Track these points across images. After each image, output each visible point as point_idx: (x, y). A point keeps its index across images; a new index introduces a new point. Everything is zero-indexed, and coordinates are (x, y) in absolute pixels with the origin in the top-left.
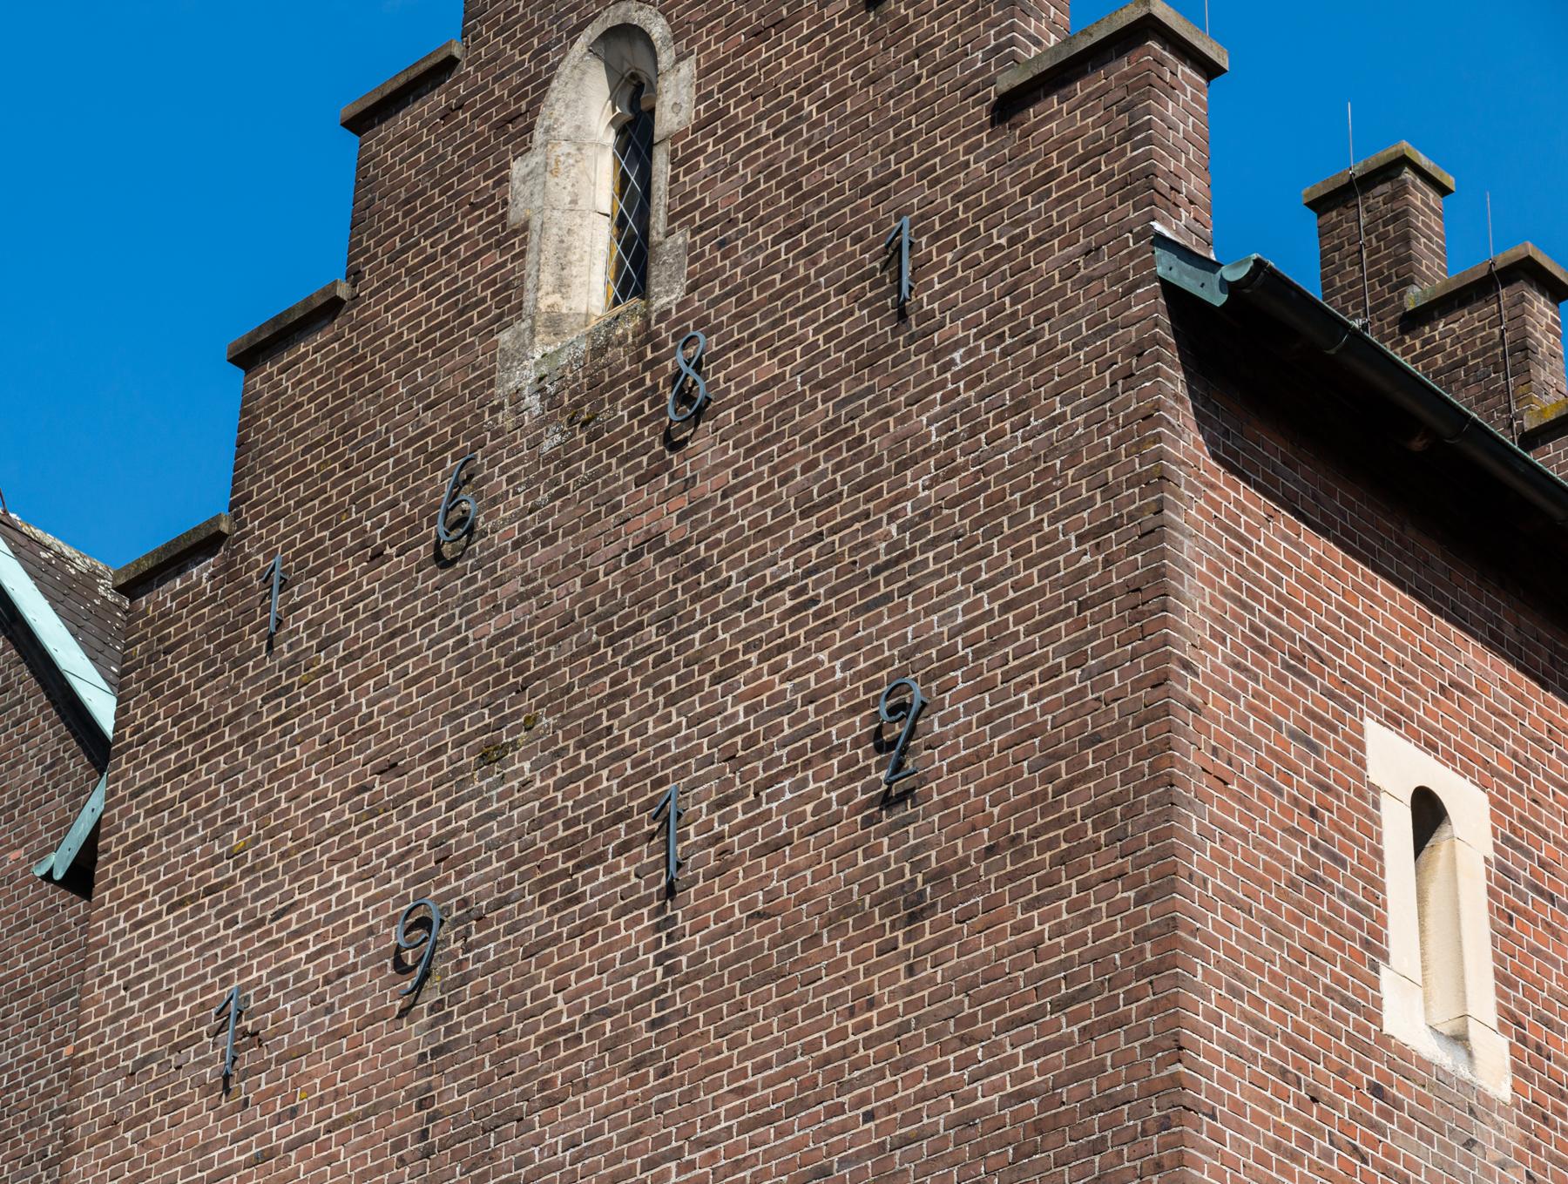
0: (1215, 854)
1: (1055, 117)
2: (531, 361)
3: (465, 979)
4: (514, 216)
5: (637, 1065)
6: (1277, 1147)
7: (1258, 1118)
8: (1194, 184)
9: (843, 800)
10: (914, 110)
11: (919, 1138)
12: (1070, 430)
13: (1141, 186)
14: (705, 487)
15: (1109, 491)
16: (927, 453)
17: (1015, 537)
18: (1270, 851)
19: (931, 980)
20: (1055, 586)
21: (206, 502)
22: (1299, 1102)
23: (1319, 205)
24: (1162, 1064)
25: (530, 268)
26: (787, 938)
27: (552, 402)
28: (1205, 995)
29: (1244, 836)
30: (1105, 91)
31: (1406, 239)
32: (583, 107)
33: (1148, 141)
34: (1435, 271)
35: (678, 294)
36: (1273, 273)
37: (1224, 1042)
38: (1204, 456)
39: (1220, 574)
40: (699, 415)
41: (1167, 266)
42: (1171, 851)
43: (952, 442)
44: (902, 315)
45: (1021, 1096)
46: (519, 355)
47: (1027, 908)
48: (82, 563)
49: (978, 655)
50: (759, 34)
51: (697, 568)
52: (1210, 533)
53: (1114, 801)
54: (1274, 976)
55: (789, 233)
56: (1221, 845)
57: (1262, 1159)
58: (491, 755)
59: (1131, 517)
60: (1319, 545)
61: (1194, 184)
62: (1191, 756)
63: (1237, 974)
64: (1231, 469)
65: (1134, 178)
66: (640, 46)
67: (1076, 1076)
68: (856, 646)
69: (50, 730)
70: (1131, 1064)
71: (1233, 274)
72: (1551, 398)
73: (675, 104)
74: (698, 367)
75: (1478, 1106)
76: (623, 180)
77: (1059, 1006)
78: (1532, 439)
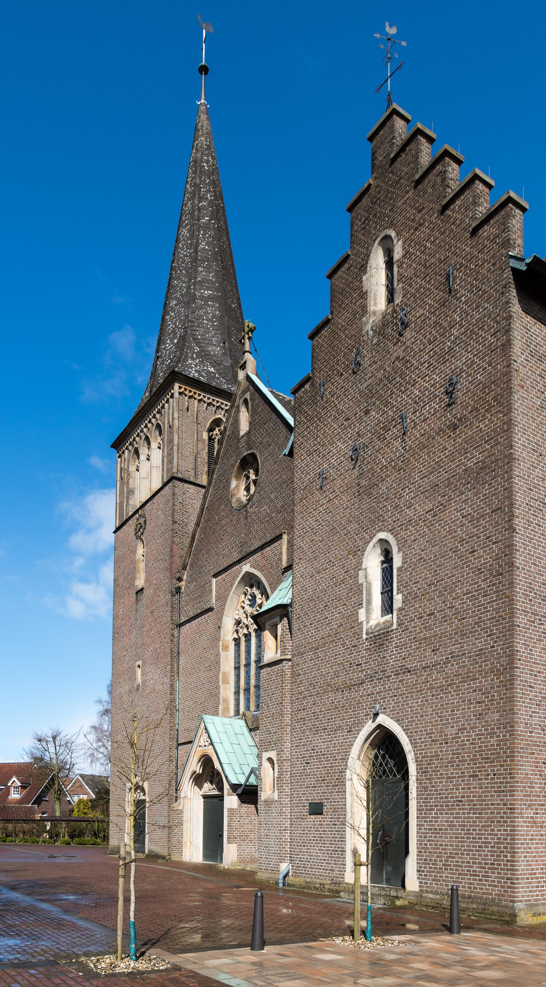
0: (521, 404)
1: (487, 231)
2: (370, 322)
3: (365, 459)
4: (364, 290)
5: (399, 470)
6: (532, 466)
7: (528, 460)
8: (519, 241)
9: (439, 407)
10: (452, 239)
11: (456, 475)
12: (489, 310)
13: (507, 244)
14: (408, 343)
15: (498, 323)
16: (456, 324)
17: (476, 339)
18: (533, 402)
19: (459, 442)
20: (485, 348)
21: (307, 371)
22: (537, 456)
24: (508, 451)
25: (368, 301)
26: (428, 439)
27: (375, 331)
28: (518, 435)
29: (527, 399)
30: (498, 221)
32: (378, 259)
33: (508, 231)
35: (400, 299)
37: (521, 444)
39: (523, 338)
40: (406, 327)
41: (513, 263)
42: (511, 404)
43: (462, 320)
44: (450, 291)
45: (478, 463)
46: (367, 322)
47: (479, 422)
49: (468, 368)
50: (416, 229)
51: (407, 362)
52: (521, 329)
53: (498, 395)
54: (533, 430)
55: (424, 278)
57: (529, 468)
58: (367, 412)
59: (503, 328)
61: (519, 241)
62: (516, 382)
63: (525, 430)
64: (526, 313)
65: (505, 242)
66: (389, 240)
67: (489, 456)
68: (441, 372)
69: (282, 426)
70: (501, 452)
71: (528, 261)
73: (398, 253)
74: (405, 316)
76: (387, 276)
77: (485, 442)
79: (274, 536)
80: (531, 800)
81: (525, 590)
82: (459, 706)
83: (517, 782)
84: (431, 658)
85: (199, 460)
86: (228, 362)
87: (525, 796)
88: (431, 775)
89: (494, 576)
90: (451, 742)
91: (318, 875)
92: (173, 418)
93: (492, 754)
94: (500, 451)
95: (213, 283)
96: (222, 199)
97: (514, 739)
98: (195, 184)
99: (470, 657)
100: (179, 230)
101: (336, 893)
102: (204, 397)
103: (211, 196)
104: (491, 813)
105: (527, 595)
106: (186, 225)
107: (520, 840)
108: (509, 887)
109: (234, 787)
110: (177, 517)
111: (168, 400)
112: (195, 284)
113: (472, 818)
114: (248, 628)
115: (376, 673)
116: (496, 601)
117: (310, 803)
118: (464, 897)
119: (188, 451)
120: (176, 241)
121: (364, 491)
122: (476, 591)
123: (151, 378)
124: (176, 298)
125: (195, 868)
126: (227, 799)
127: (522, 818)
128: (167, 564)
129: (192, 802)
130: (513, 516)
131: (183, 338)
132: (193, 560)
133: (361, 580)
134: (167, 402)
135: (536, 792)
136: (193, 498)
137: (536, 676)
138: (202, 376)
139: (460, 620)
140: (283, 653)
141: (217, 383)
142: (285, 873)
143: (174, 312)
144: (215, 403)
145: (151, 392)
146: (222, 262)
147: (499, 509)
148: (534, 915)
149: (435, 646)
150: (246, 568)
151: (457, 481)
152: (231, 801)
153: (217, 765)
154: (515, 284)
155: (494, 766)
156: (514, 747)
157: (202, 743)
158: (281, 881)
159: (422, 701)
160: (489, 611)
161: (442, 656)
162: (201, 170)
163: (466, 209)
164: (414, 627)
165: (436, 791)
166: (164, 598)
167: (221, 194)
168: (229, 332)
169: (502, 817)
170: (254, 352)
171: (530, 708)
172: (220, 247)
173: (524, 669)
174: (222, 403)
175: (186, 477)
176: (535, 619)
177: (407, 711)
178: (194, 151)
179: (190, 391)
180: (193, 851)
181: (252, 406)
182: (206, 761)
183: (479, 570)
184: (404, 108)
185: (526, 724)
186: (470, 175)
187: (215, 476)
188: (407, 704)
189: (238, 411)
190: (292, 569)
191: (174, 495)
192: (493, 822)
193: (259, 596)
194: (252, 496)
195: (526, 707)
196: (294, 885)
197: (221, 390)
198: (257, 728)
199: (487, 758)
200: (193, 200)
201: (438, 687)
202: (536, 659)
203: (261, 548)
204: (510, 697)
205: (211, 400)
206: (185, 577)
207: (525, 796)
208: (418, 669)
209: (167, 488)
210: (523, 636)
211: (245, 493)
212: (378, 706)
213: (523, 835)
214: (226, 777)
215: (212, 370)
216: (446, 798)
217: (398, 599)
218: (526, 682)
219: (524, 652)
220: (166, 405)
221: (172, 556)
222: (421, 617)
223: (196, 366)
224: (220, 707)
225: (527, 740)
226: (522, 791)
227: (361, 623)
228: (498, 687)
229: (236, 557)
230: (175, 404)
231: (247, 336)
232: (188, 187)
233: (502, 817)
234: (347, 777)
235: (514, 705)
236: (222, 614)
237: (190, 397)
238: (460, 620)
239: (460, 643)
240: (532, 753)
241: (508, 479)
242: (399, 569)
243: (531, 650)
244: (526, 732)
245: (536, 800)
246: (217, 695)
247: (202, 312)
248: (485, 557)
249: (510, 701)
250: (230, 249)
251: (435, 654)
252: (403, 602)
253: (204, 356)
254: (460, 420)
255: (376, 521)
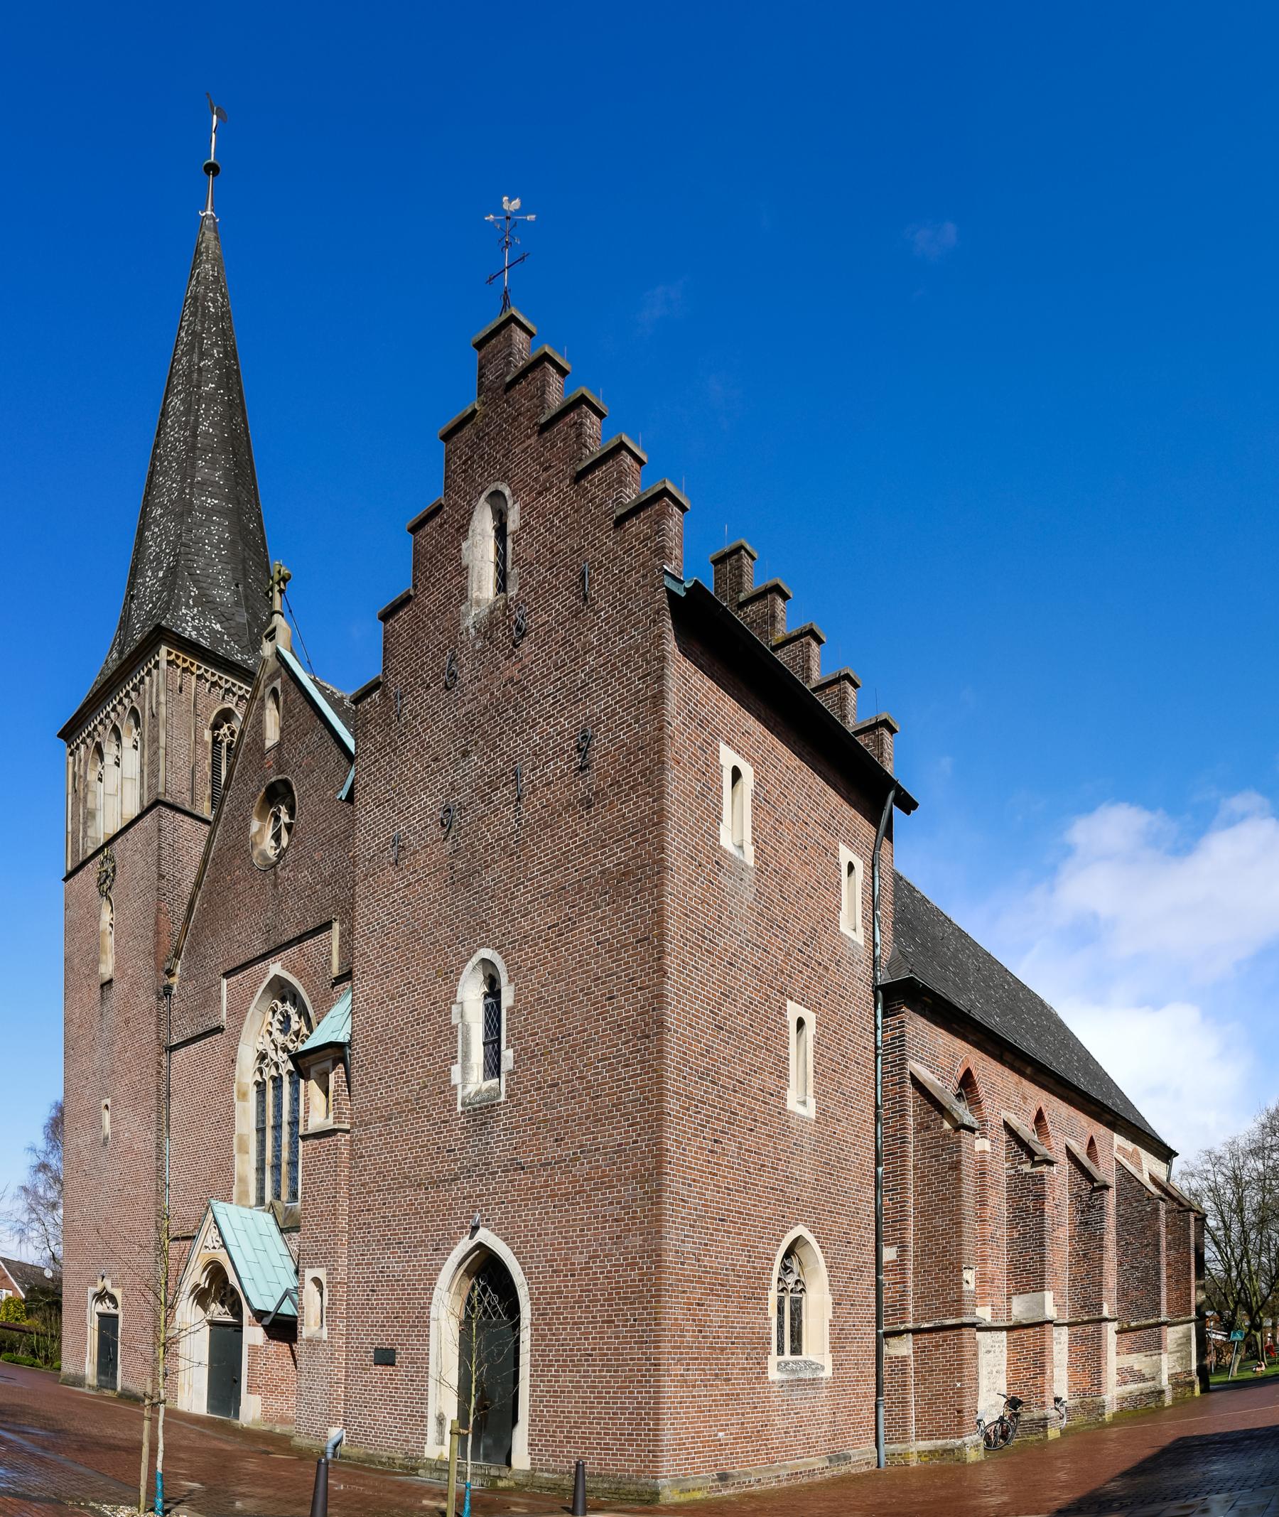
1: (636, 526)
2: (472, 616)
21: (375, 672)
23: (715, 562)
27: (478, 631)
30: (650, 516)
31: (741, 576)
32: (484, 522)
34: (751, 586)
35: (516, 591)
36: (700, 585)
38: (677, 651)
41: (669, 583)
44: (585, 599)
45: (619, 864)
46: (467, 614)
48: (339, 695)
50: (540, 494)
56: (677, 782)
57: (685, 884)
58: (465, 754)
60: (710, 683)
61: (677, 552)
62: (670, 754)
67: (634, 858)
69: (336, 751)
71: (688, 586)
72: (780, 635)
73: (513, 522)
75: (745, 868)
76: (498, 549)
78: (775, 648)
79: (318, 923)
80: (681, 1353)
81: (678, 1063)
82: (591, 1224)
83: (664, 1330)
84: (553, 1152)
85: (198, 775)
86: (243, 618)
87: (673, 1347)
88: (551, 1319)
89: (639, 1039)
90: (580, 1275)
91: (385, 1443)
92: (158, 703)
93: (632, 1293)
94: (648, 852)
95: (219, 487)
96: (235, 358)
97: (661, 1272)
98: (194, 332)
99: (606, 1154)
100: (166, 399)
101: (414, 1470)
102: (207, 671)
103: (219, 353)
104: (630, 1370)
105: (680, 1070)
106: (179, 392)
107: (666, 1404)
108: (650, 1461)
109: (259, 1315)
110: (165, 868)
111: (150, 670)
112: (191, 485)
113: (605, 1377)
114: (277, 1068)
115: (477, 1166)
116: (640, 1075)
117: (376, 1349)
118: (592, 1475)
119: (182, 759)
120: (162, 415)
121: (461, 880)
122: (614, 1057)
123: (120, 629)
124: (162, 505)
125: (197, 1420)
126: (247, 1329)
127: (670, 1375)
128: (149, 944)
129: (193, 1327)
130: (663, 952)
131: (172, 571)
132: (191, 942)
133: (455, 1020)
134: (149, 673)
135: (688, 1342)
136: (190, 840)
137: (690, 1185)
138: (202, 636)
139: (592, 1099)
140: (337, 1119)
141: (225, 649)
142: (336, 1440)
143: (158, 526)
144: (222, 683)
145: (121, 653)
146: (235, 455)
147: (646, 939)
148: (682, 1491)
149: (559, 1134)
150: (275, 968)
151: (591, 888)
152: (253, 1335)
153: (232, 1279)
154: (671, 611)
155: (635, 1309)
156: (661, 1284)
157: (209, 1243)
158: (330, 1451)
159: (540, 1214)
160: (631, 1089)
161: (569, 1149)
162: (203, 312)
163: (610, 486)
164: (530, 1102)
165: (557, 1340)
166: (146, 1000)
167: (235, 350)
168: (244, 568)
169: (643, 1376)
170: (288, 613)
171: (683, 1230)
172: (232, 431)
173: (675, 1176)
174: (234, 685)
175: (178, 802)
176: (690, 1105)
177: (519, 1227)
178: (194, 282)
179: (185, 660)
180: (193, 1396)
181: (285, 702)
182: (216, 1271)
183: (619, 1026)
184: (526, 316)
185: (677, 1252)
186: (614, 442)
187: (225, 809)
188: (520, 1216)
189: (262, 707)
190: (350, 979)
191: (160, 830)
192: (632, 1382)
193: (295, 1018)
194: (285, 850)
195: (677, 1229)
196: (349, 1458)
197: (232, 662)
198: (296, 1229)
199: (625, 1298)
200: (191, 356)
201: (562, 1195)
202: (690, 1162)
203: (299, 939)
204: (656, 1215)
205: (216, 678)
206: (178, 971)
207: (673, 1347)
208: (535, 1166)
209: (148, 817)
210: (675, 1129)
211: (273, 843)
212: (478, 1216)
213: (670, 1397)
214: (247, 1299)
215: (218, 627)
216: (571, 1350)
217: (508, 1055)
218: (677, 1194)
219: (675, 1152)
220: (147, 679)
221: (157, 933)
222: (540, 1088)
223: (193, 619)
224: (235, 1189)
225: (677, 1274)
226: (670, 1341)
227: (455, 1087)
228: (642, 1199)
229: (259, 949)
230: (161, 679)
231: (277, 588)
232: (183, 334)
233: (643, 1376)
234: (432, 1315)
235: (661, 1226)
236: (238, 1039)
237: (185, 670)
238: (592, 1099)
239: (593, 1133)
240: (684, 1292)
241: (659, 897)
242: (509, 1010)
243: (684, 1149)
244: (676, 1263)
245: (687, 1353)
246: (229, 1170)
247: (202, 532)
248: (626, 1008)
249: (657, 1221)
250: (247, 435)
251: (559, 1146)
252: (515, 1062)
253: (206, 603)
254: (596, 794)
255: (478, 931)
